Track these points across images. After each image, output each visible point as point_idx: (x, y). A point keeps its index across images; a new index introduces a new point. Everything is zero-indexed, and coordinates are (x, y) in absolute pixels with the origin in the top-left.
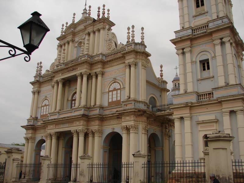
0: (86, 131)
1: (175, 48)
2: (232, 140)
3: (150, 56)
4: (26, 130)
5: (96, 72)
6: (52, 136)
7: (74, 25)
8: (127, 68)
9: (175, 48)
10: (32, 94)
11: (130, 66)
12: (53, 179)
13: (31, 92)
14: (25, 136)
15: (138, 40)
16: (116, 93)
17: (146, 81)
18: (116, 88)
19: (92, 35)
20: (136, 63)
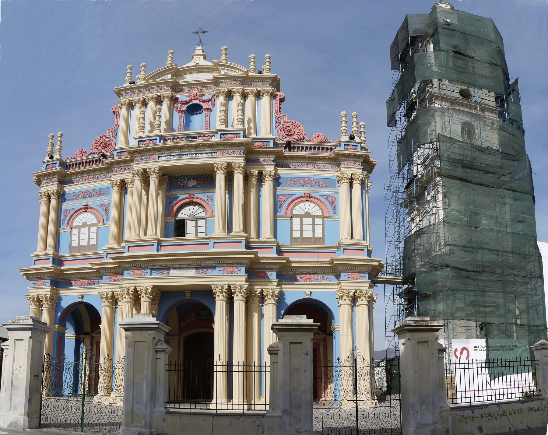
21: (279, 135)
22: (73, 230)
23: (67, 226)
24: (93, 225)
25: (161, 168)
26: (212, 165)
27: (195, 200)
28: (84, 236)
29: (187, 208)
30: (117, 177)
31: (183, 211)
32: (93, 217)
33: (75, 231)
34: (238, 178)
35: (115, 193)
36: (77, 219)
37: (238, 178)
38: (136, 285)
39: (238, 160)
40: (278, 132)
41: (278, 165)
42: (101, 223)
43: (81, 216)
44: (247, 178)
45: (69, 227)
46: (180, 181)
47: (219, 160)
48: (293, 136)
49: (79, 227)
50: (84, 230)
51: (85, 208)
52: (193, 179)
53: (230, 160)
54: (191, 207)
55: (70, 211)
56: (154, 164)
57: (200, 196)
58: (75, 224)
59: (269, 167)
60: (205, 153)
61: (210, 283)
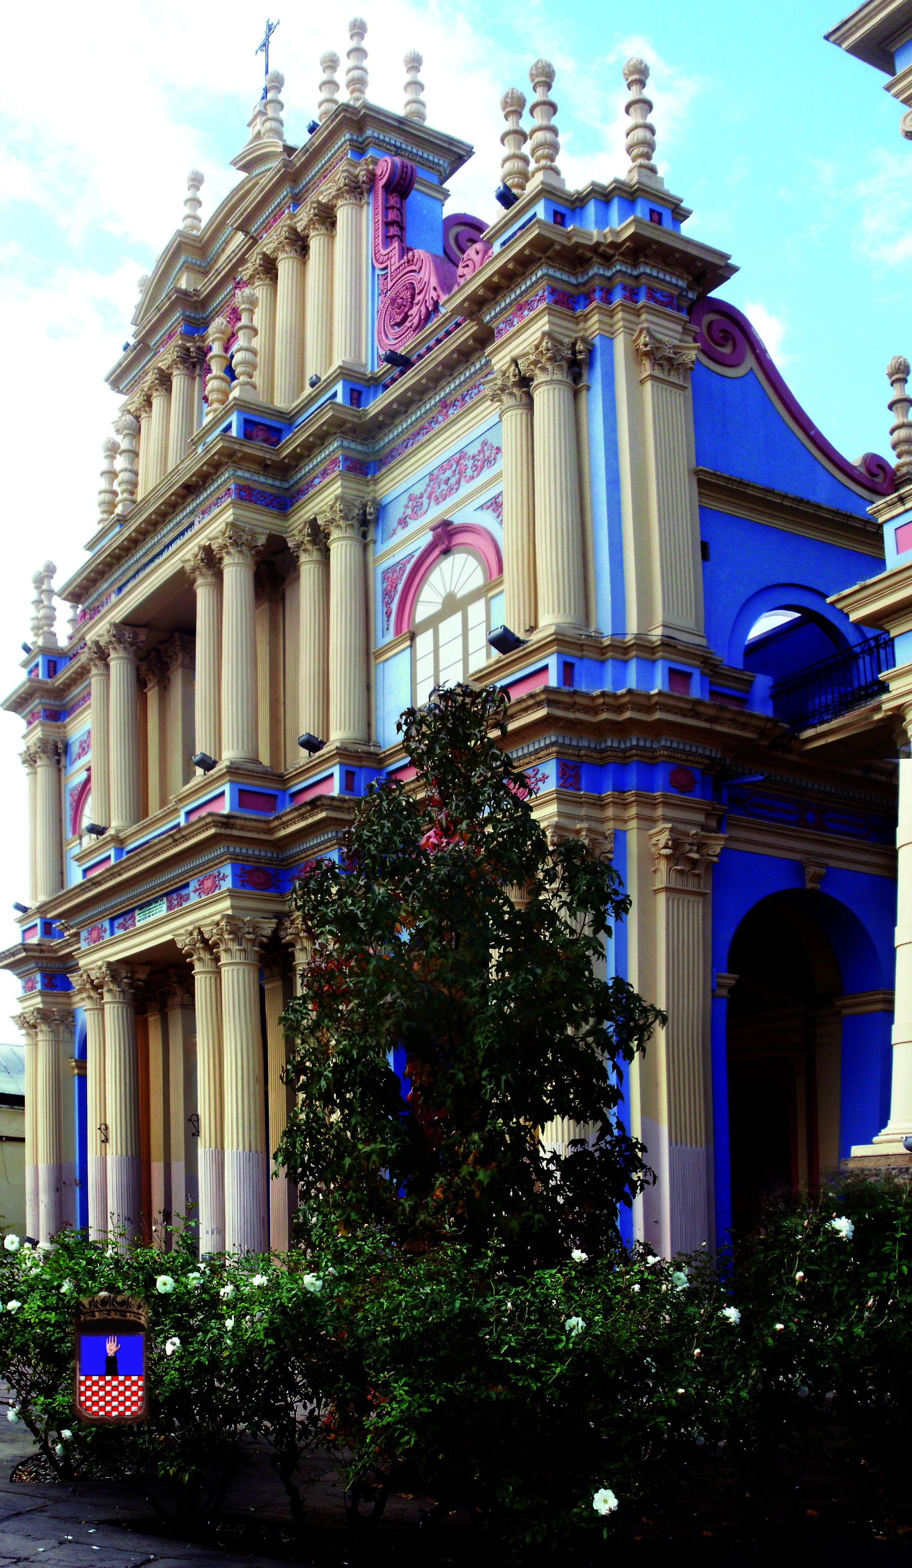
0: (268, 932)
1: (888, 88)
2: (251, 142)
3: (725, 279)
4: (20, 975)
5: (313, 523)
6: (216, 945)
7: (192, 249)
8: (510, 408)
9: (888, 88)
10: (25, 770)
11: (525, 382)
12: (708, 815)
13: (19, 760)
14: (18, 1009)
15: (591, 160)
16: (459, 631)
17: (701, 483)
18: (459, 595)
19: (285, 267)
20: (580, 346)
22: (419, 640)
28: (451, 653)
32: (472, 562)
33: (424, 641)
48: (408, 324)
49: (433, 622)
50: (451, 627)
55: (402, 564)
58: (422, 612)
61: (169, 937)
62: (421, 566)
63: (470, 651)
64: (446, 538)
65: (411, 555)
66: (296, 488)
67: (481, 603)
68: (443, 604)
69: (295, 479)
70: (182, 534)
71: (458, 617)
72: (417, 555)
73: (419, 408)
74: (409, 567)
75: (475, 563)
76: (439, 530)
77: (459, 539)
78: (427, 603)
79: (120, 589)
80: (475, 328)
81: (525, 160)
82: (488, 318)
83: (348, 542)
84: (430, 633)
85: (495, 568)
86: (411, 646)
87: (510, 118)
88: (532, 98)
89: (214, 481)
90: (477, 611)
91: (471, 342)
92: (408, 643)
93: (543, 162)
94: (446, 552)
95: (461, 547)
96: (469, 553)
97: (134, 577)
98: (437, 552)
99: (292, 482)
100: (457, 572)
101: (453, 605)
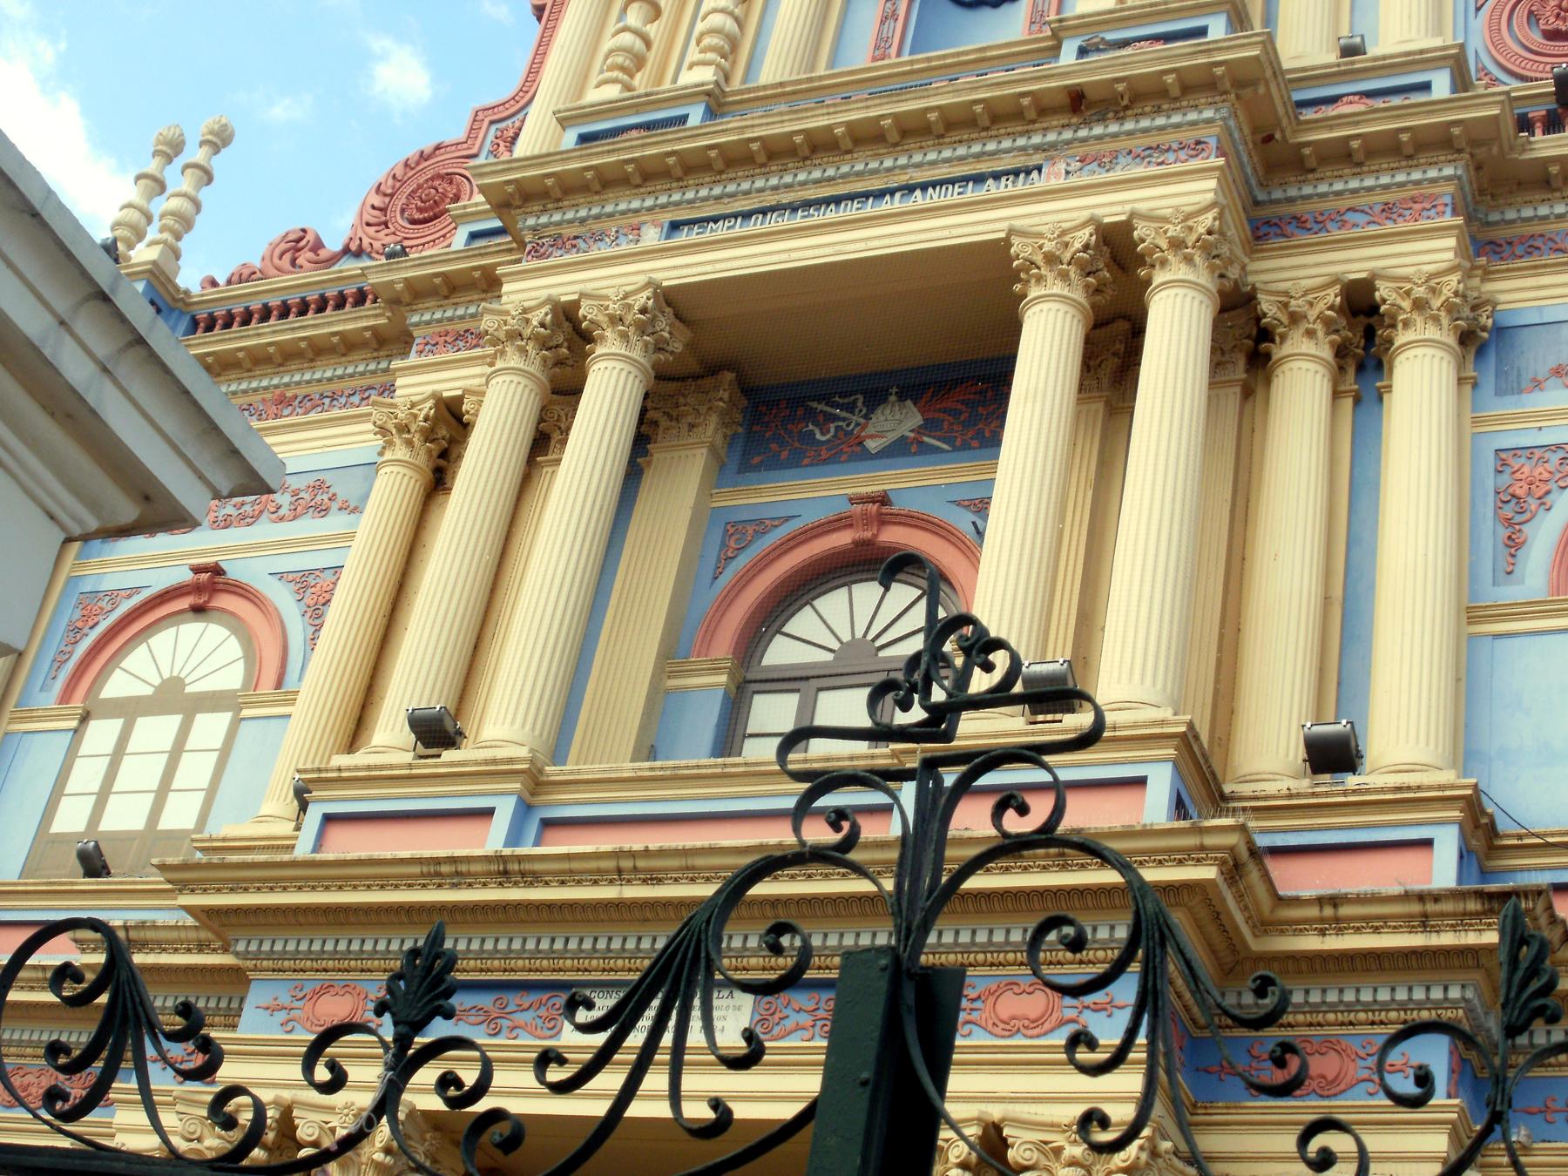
18: (188, 689)
21: (1497, 43)
22: (94, 726)
23: (66, 696)
24: (213, 701)
25: (672, 301)
26: (995, 254)
27: (896, 536)
28: (140, 772)
29: (833, 604)
30: (419, 383)
31: (803, 622)
32: (234, 648)
33: (102, 734)
34: (1176, 325)
35: (394, 486)
36: (137, 659)
37: (1176, 325)
38: (995, 1112)
39: (1174, 192)
40: (1494, 29)
41: (1487, 245)
42: (266, 688)
43: (162, 641)
44: (1245, 343)
45: (77, 703)
46: (811, 415)
47: (1049, 209)
49: (130, 710)
50: (156, 732)
51: (196, 588)
52: (902, 398)
53: (1112, 207)
54: (867, 592)
55: (114, 596)
56: (623, 270)
57: (917, 484)
58: (117, 686)
59: (1417, 255)
60: (965, 180)
62: (154, 609)
63: (175, 786)
64: (207, 591)
65: (138, 590)
66: (1298, 209)
67: (225, 718)
68: (158, 689)
69: (1292, 192)
70: (979, 179)
71: (173, 722)
72: (145, 595)
73: (240, 380)
74: (125, 606)
75: (239, 652)
76: (205, 577)
77: (225, 601)
78: (134, 673)
79: (675, 226)
80: (383, 321)
81: (149, 219)
82: (415, 319)
83: (409, 472)
84: (116, 724)
85: (271, 679)
86: (76, 731)
87: (158, 159)
88: (195, 153)
89: (1158, 111)
90: (210, 728)
91: (368, 334)
92: (74, 724)
93: (166, 236)
94: (199, 610)
95: (225, 617)
96: (234, 631)
97: (793, 208)
98: (185, 603)
99: (1278, 194)
100: (202, 652)
101: (174, 698)
